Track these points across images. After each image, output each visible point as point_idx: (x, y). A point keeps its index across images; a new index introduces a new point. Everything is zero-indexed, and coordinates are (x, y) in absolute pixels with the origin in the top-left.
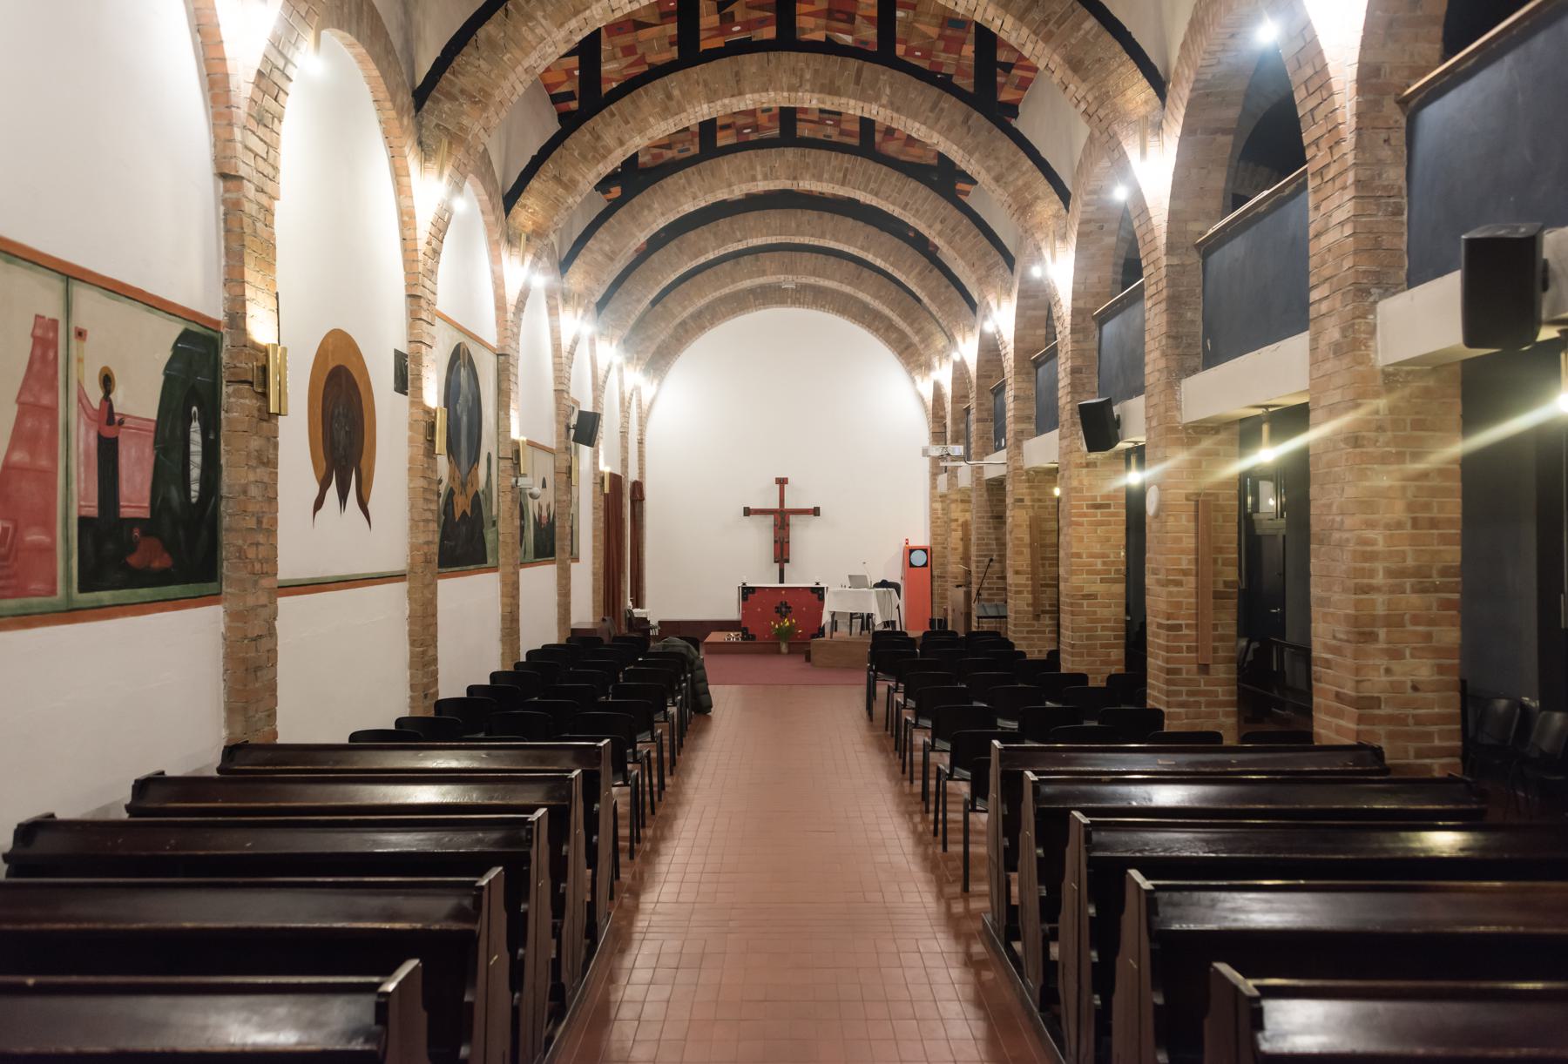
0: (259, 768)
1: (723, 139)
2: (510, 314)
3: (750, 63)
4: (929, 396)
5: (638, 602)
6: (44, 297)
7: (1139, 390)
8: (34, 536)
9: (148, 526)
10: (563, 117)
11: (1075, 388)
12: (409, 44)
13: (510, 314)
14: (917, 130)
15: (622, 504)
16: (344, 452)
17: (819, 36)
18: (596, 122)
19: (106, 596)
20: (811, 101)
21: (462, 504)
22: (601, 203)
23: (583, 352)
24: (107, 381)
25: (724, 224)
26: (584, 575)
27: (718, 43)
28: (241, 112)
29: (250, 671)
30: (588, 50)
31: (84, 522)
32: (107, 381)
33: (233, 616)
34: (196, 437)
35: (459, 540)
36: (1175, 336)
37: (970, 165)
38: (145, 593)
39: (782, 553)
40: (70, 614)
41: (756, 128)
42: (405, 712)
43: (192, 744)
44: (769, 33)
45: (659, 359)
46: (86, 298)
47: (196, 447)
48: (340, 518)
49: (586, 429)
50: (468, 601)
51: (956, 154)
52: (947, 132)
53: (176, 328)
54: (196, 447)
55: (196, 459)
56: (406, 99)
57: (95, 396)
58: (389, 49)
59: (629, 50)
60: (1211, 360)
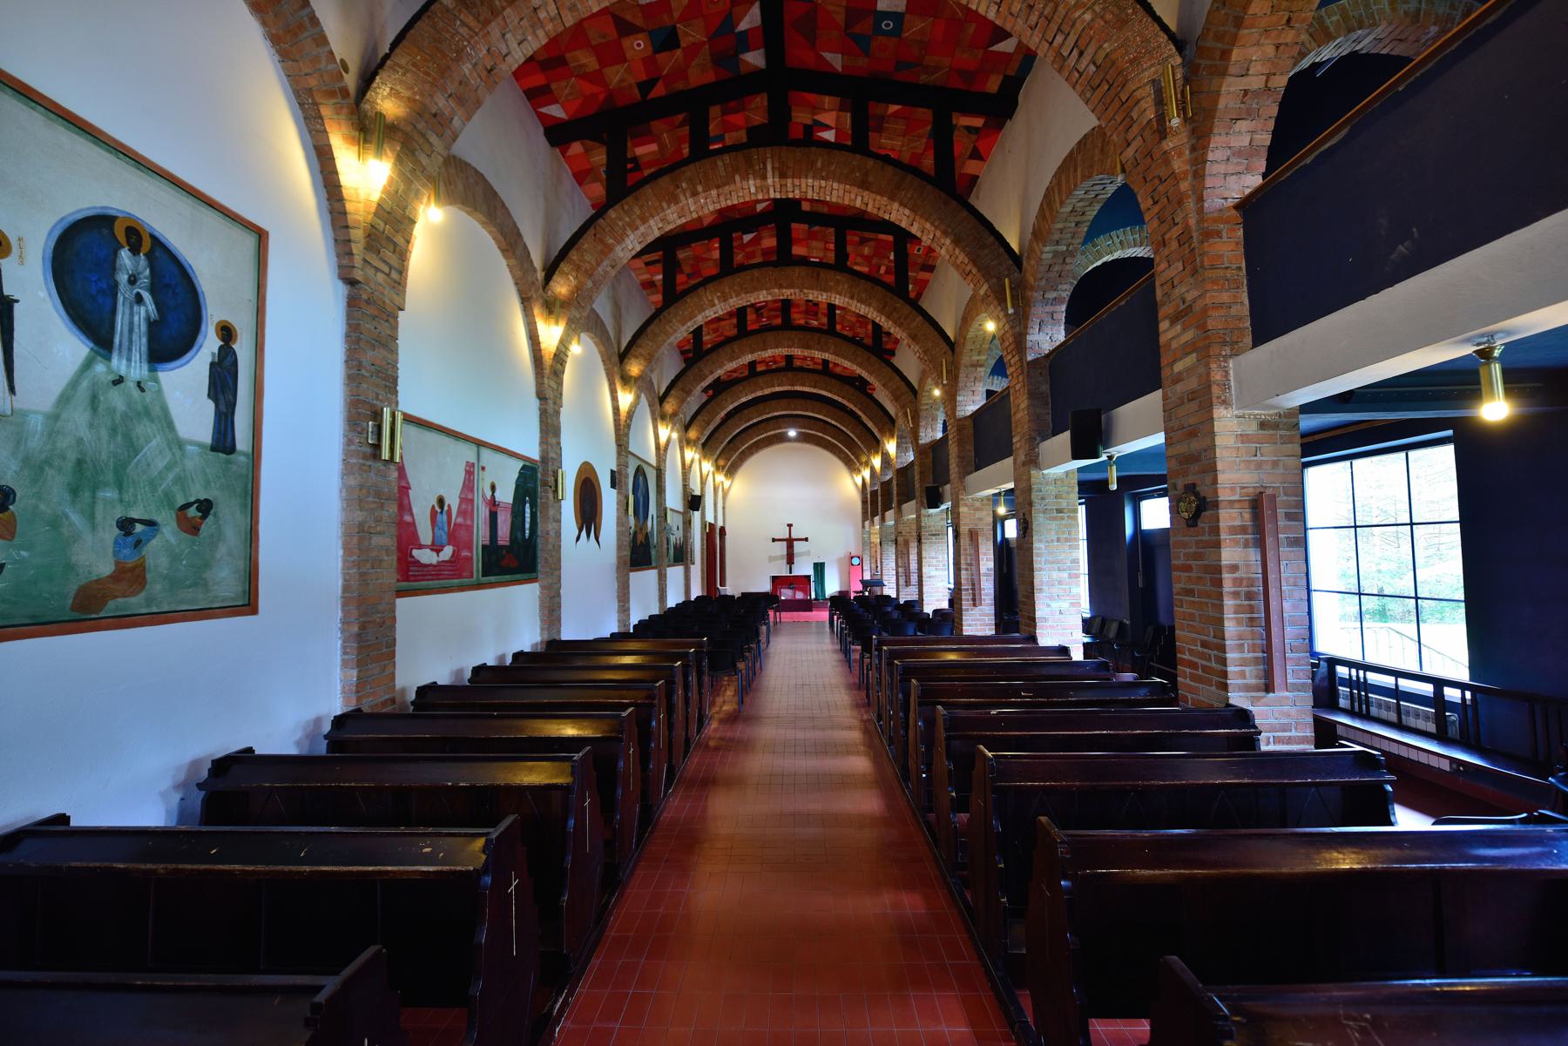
0: (557, 656)
1: (760, 368)
2: (661, 451)
3: (770, 336)
4: (860, 483)
5: (723, 583)
6: (468, 453)
7: (948, 482)
8: (465, 553)
9: (509, 549)
10: (686, 360)
11: (921, 480)
12: (619, 332)
13: (661, 451)
14: (847, 364)
15: (715, 537)
16: (589, 515)
17: (802, 322)
18: (701, 364)
19: (492, 579)
20: (797, 352)
21: (640, 538)
22: (705, 398)
23: (696, 467)
24: (493, 488)
25: (761, 406)
26: (697, 571)
27: (756, 327)
28: (547, 372)
29: (551, 610)
30: (697, 332)
31: (484, 547)
32: (493, 488)
33: (543, 588)
34: (528, 510)
35: (638, 554)
36: (961, 458)
37: (871, 379)
38: (508, 577)
39: (790, 559)
40: (479, 586)
41: (775, 362)
42: (616, 630)
43: (528, 638)
44: (778, 321)
45: (731, 471)
46: (485, 452)
47: (528, 515)
48: (586, 543)
49: (694, 502)
50: (643, 581)
51: (865, 374)
52: (860, 365)
53: (520, 464)
54: (528, 515)
55: (528, 520)
56: (616, 359)
57: (489, 494)
58: (608, 338)
59: (715, 331)
60: (978, 468)
